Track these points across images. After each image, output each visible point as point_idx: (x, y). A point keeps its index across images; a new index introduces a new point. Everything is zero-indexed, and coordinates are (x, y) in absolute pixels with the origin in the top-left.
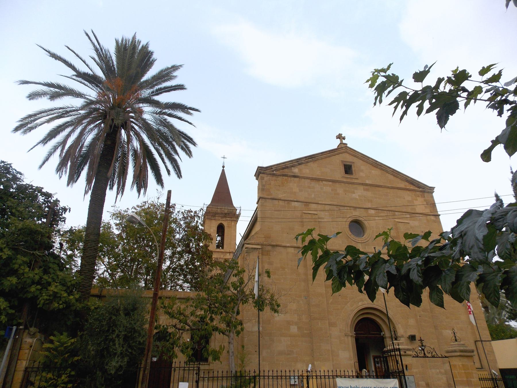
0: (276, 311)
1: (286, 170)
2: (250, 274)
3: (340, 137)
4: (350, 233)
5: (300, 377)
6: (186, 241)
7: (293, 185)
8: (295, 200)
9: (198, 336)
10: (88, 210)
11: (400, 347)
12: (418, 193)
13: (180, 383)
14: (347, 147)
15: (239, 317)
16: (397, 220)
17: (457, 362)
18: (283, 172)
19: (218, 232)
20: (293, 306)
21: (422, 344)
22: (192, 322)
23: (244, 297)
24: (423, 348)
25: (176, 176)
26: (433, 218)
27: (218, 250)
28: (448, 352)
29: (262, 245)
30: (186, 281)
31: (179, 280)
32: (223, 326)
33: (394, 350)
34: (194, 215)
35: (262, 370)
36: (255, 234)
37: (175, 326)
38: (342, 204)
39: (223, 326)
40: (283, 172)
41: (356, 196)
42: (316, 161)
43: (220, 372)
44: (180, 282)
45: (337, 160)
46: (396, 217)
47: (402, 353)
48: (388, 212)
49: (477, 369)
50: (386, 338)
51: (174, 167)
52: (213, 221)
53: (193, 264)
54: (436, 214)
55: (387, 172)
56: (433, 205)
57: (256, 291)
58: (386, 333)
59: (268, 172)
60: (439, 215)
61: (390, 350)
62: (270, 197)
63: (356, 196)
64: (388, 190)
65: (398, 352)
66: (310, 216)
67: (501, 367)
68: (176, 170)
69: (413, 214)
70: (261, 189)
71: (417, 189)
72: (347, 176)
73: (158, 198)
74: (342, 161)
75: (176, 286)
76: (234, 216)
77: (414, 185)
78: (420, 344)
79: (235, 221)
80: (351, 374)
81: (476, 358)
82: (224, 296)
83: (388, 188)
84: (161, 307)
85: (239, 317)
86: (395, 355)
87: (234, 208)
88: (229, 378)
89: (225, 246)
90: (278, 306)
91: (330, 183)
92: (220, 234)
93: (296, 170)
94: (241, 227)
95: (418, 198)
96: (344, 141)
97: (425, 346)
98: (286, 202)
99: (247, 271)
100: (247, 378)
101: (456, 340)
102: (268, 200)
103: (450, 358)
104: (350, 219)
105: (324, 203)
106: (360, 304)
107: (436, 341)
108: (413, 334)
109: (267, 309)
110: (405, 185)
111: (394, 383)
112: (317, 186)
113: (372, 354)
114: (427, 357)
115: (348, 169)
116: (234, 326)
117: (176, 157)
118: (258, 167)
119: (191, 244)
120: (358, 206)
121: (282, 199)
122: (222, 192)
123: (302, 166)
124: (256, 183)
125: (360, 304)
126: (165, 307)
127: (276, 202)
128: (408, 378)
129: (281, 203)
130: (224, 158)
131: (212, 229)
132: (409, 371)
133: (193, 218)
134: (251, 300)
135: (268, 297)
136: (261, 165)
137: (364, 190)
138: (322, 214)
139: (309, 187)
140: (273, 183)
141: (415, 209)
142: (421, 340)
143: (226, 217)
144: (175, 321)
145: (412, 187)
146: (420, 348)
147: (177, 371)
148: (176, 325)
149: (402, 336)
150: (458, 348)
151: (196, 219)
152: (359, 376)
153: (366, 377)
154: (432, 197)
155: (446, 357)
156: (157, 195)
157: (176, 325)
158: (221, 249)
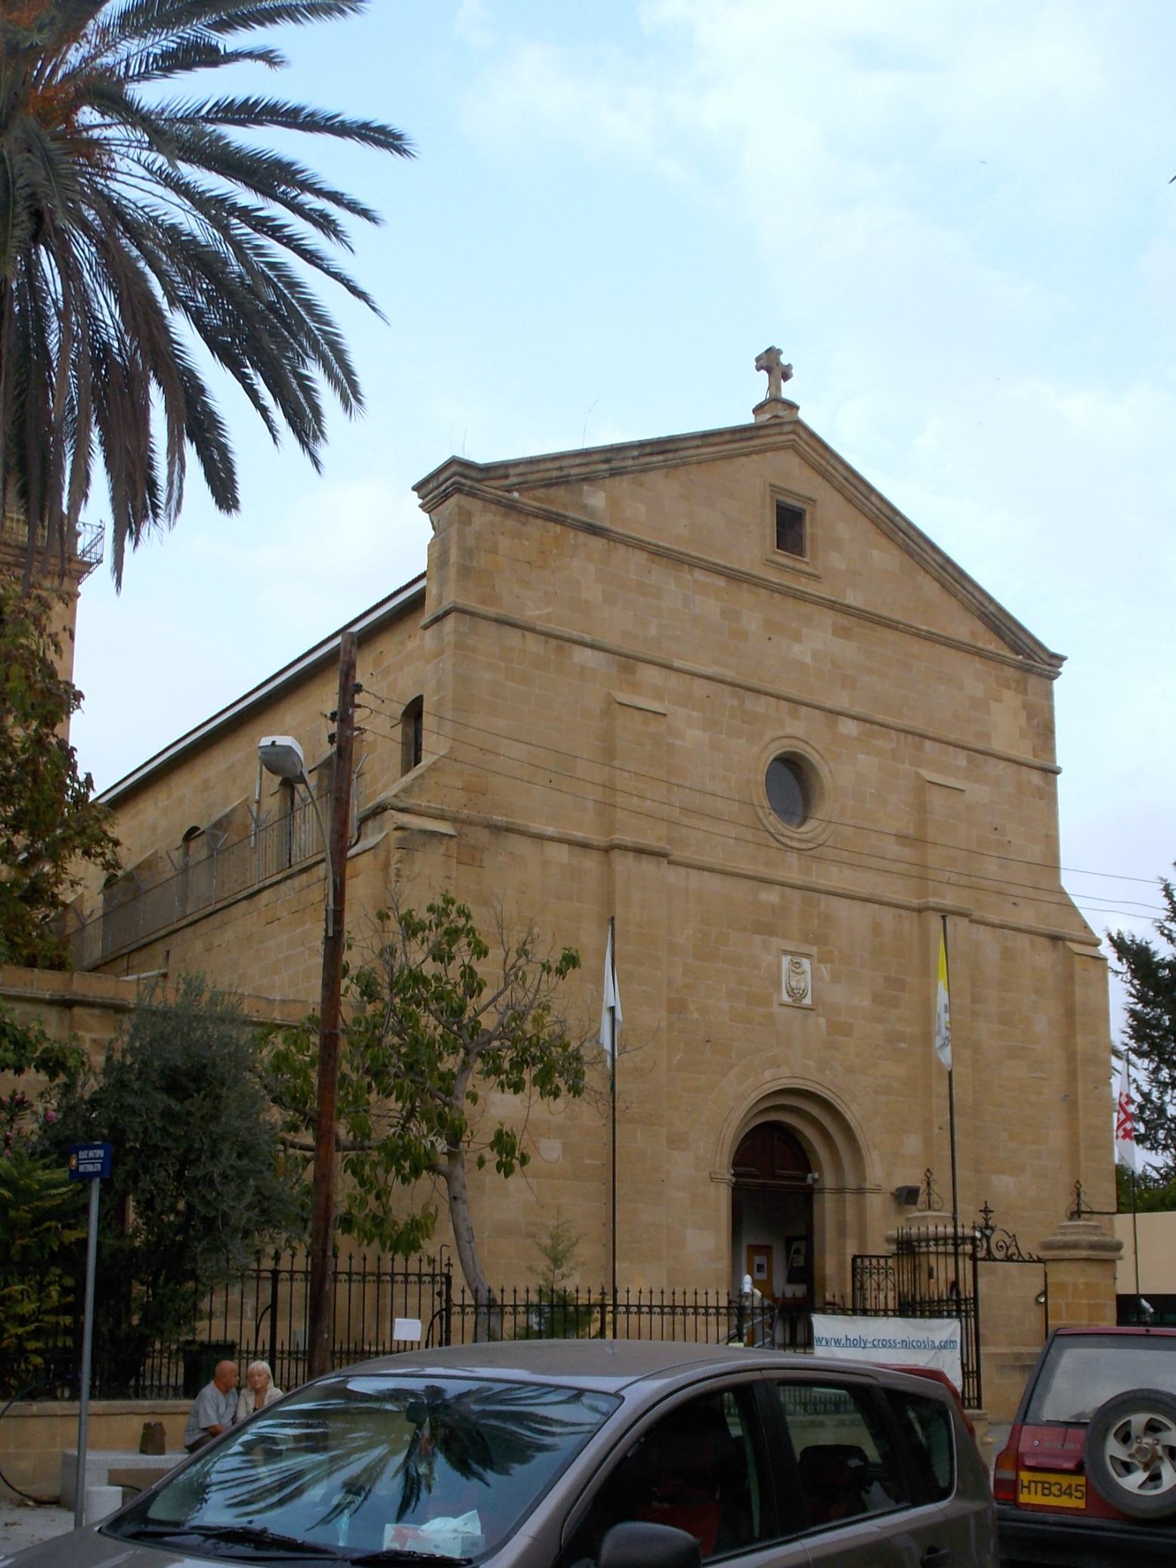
1: (559, 493)
3: (771, 364)
4: (766, 803)
7: (583, 566)
8: (588, 638)
12: (1009, 672)
13: (397, 1320)
16: (929, 776)
18: (550, 501)
21: (987, 1220)
22: (504, 1143)
24: (988, 1232)
26: (1036, 778)
28: (1048, 1246)
38: (754, 682)
40: (550, 501)
41: (803, 651)
42: (676, 467)
45: (758, 476)
50: (822, 1190)
54: (1047, 764)
56: (1045, 732)
59: (490, 488)
60: (1056, 772)
62: (492, 611)
63: (803, 651)
64: (915, 646)
67: (1121, 1292)
71: (1007, 653)
72: (784, 559)
74: (775, 489)
77: (1002, 637)
91: (721, 582)
93: (596, 500)
96: (788, 391)
98: (553, 643)
100: (571, 1309)
102: (483, 625)
103: (1050, 1266)
105: (688, 666)
106: (768, 1074)
110: (973, 634)
111: (949, 1331)
114: (995, 1260)
115: (789, 526)
120: (807, 698)
121: (540, 625)
125: (768, 1074)
127: (513, 637)
129: (534, 645)
140: (504, 543)
145: (993, 645)
154: (1049, 695)
155: (1039, 1260)
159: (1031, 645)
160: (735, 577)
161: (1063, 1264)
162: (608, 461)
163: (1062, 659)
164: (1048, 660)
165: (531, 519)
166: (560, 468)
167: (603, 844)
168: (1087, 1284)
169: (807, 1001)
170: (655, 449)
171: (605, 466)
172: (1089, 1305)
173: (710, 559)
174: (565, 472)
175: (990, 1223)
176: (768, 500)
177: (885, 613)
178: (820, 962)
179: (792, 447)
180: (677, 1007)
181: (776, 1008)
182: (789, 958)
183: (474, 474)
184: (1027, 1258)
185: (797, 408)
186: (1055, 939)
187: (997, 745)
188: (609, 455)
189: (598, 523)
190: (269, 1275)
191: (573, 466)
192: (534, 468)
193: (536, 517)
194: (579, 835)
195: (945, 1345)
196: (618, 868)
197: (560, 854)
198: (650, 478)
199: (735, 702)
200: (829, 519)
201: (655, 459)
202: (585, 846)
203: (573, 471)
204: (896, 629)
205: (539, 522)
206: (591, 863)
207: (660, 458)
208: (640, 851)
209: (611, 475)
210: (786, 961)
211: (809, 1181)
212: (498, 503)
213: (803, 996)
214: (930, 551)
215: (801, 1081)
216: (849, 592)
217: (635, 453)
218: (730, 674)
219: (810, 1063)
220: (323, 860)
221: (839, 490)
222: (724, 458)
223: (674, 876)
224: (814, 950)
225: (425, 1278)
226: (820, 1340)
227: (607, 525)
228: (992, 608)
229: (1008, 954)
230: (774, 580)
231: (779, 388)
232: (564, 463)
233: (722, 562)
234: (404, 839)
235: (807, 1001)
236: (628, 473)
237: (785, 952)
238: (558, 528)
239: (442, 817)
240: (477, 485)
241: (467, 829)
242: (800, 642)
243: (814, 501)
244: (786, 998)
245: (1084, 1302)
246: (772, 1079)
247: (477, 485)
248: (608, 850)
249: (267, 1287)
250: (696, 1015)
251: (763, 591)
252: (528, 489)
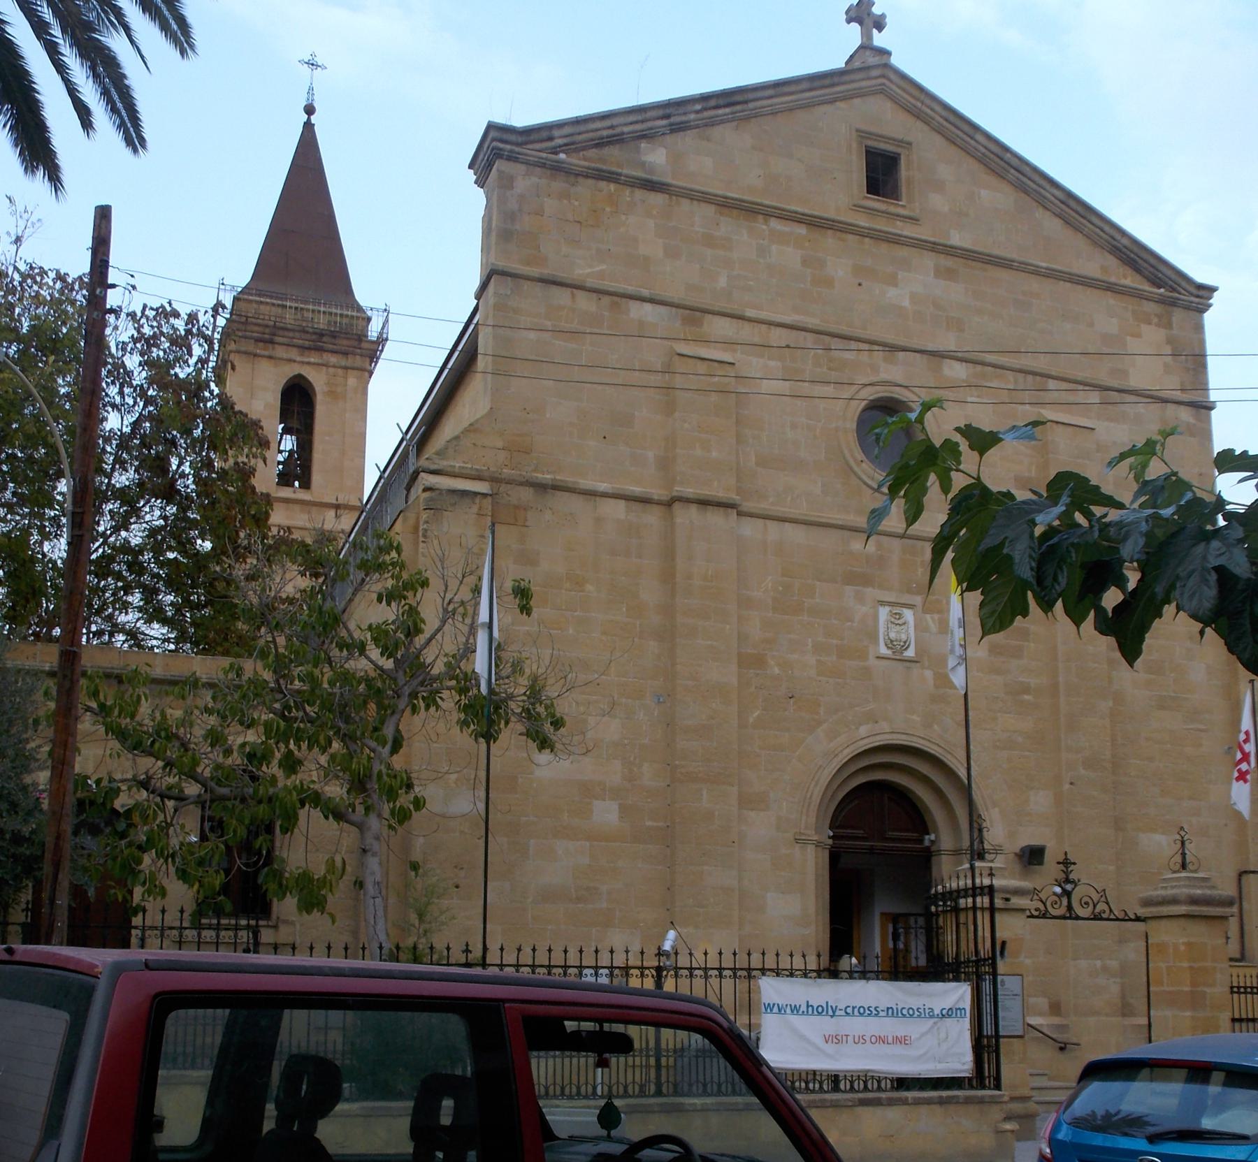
0: (544, 743)
1: (613, 152)
2: (449, 596)
3: (864, 15)
4: (860, 455)
5: (616, 972)
6: (149, 449)
7: (641, 222)
8: (645, 293)
9: (240, 821)
11: (997, 882)
14: (888, 66)
15: (398, 762)
17: (1170, 935)
20: (610, 730)
21: (1067, 873)
23: (422, 684)
24: (1069, 887)
25: (117, 139)
26: (1185, 415)
27: (286, 492)
28: (1147, 903)
29: (494, 480)
30: (154, 613)
31: (125, 607)
32: (335, 790)
33: (975, 891)
34: (188, 332)
35: (493, 947)
36: (467, 431)
37: (145, 784)
38: (844, 329)
39: (335, 790)
42: (747, 119)
43: (699, 956)
44: (128, 618)
46: (1048, 397)
47: (999, 903)
48: (1020, 376)
49: (1231, 960)
51: (105, 93)
52: (264, 365)
53: (184, 546)
55: (1042, 203)
56: (1196, 361)
57: (480, 664)
58: (944, 837)
59: (531, 152)
60: (1210, 407)
61: (958, 891)
62: (534, 271)
64: (1035, 284)
65: (986, 900)
66: (702, 368)
68: (114, 110)
69: (1115, 394)
70: (501, 230)
71: (1147, 287)
72: (875, 203)
73: (18, 240)
74: (862, 134)
75: (111, 635)
76: (357, 346)
77: (1138, 270)
78: (1062, 876)
79: (363, 370)
80: (798, 963)
81: (1233, 924)
82: (346, 678)
83: (1037, 272)
84: (88, 709)
85: (398, 762)
86: (974, 908)
87: (360, 309)
88: (697, 972)
89: (316, 478)
90: (558, 723)
91: (802, 230)
92: (295, 425)
93: (656, 157)
94: (391, 401)
95: (1144, 327)
96: (879, 39)
98: (606, 300)
99: (435, 583)
101: (1184, 866)
102: (526, 285)
103: (1152, 924)
104: (870, 394)
105: (763, 315)
106: (863, 730)
107: (1112, 868)
109: (511, 737)
110: (1104, 269)
112: (743, 238)
113: (884, 904)
114: (1078, 918)
115: (882, 173)
116: (381, 792)
117: (117, 43)
118: (491, 127)
119: (174, 462)
120: (901, 341)
121: (590, 283)
122: (303, 233)
123: (687, 140)
124: (478, 198)
125: (863, 730)
126: (102, 706)
127: (561, 297)
128: (1002, 981)
129: (585, 303)
130: (312, 64)
131: (257, 393)
132: (1007, 960)
133: (180, 343)
134: (448, 700)
135: (520, 688)
136: (500, 119)
137: (941, 273)
138: (754, 364)
139: (709, 241)
140: (550, 205)
141: (1124, 373)
142: (1066, 863)
143: (320, 350)
144: (147, 764)
145: (1130, 280)
146: (1058, 890)
148: (149, 778)
149: (997, 851)
150: (1186, 891)
151: (197, 351)
153: (851, 975)
154: (1199, 328)
156: (12, 226)
157: (149, 778)
158: (294, 492)
159: (1173, 276)
160: (817, 224)
161: (1164, 922)
162: (667, 117)
163: (1212, 290)
165: (581, 180)
166: (612, 127)
167: (665, 498)
168: (1189, 945)
169: (910, 653)
170: (721, 102)
171: (664, 122)
173: (788, 207)
174: (618, 130)
175: (1071, 876)
176: (854, 145)
177: (996, 252)
178: (925, 611)
179: (882, 92)
180: (751, 662)
181: (872, 661)
182: (887, 609)
183: (513, 138)
185: (889, 53)
187: (1136, 380)
188: (668, 111)
189: (655, 178)
191: (626, 125)
192: (582, 128)
193: (587, 177)
194: (637, 490)
195: (948, 1014)
196: (678, 520)
197: (617, 510)
198: (717, 132)
200: (926, 158)
201: (720, 111)
202: (645, 501)
203: (626, 129)
204: (1010, 267)
205: (590, 181)
206: (652, 518)
207: (727, 110)
208: (704, 503)
209: (672, 131)
211: (927, 843)
212: (543, 166)
213: (905, 646)
214: (1048, 187)
215: (904, 737)
216: (952, 232)
217: (698, 107)
218: (812, 322)
219: (915, 717)
221: (939, 131)
222: (801, 107)
223: (749, 529)
224: (918, 600)
226: (769, 1008)
227: (669, 180)
228: (1125, 241)
230: (862, 224)
231: (870, 37)
232: (615, 121)
233: (799, 209)
234: (431, 499)
235: (910, 653)
236: (690, 128)
237: (882, 603)
238: (612, 187)
239: (479, 478)
240: (517, 149)
241: (503, 488)
242: (896, 285)
243: (910, 144)
244: (884, 650)
245: (1185, 965)
246: (867, 736)
247: (517, 149)
248: (669, 503)
250: (777, 670)
251: (850, 237)
252: (577, 150)
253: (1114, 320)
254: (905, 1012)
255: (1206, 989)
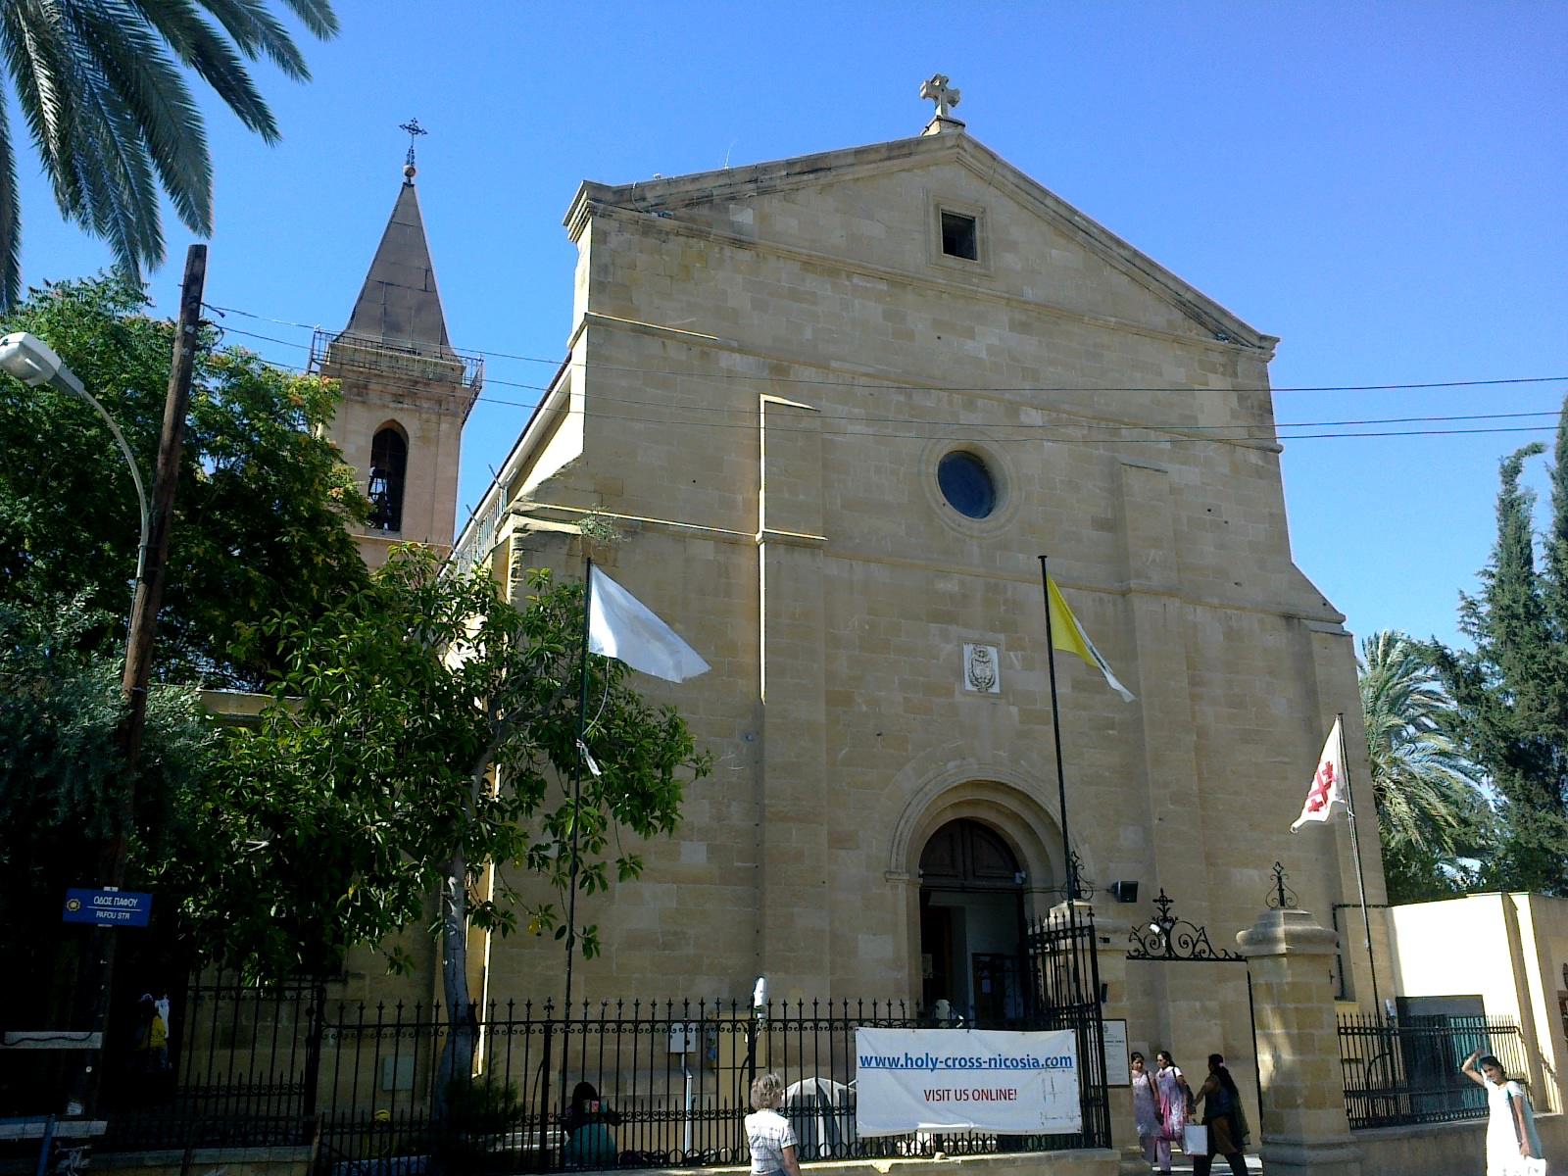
1: (704, 211)
10: (21, 202)
19: (376, 458)
24: (1167, 926)
77: (1203, 324)
91: (883, 286)
92: (387, 468)
93: (744, 217)
97: (1173, 922)
103: (1254, 964)
108: (1130, 879)
114: (1178, 958)
115: (958, 237)
123: (772, 204)
127: (652, 346)
130: (414, 130)
142: (1163, 900)
147: (208, 1005)
152: (926, 1019)
163: (1278, 340)
164: (1257, 343)
172: (1297, 1009)
178: (1008, 649)
181: (958, 698)
182: (972, 647)
184: (1221, 955)
186: (1289, 618)
190: (540, 1026)
199: (902, 398)
210: (968, 649)
211: (1018, 881)
213: (991, 683)
214: (1114, 247)
219: (1001, 753)
220: (1536, 449)
224: (1002, 637)
225: (739, 1025)
229: (1231, 635)
235: (996, 689)
249: (538, 1039)
253: (1182, 370)
254: (1008, 1063)
255: (1313, 1031)
